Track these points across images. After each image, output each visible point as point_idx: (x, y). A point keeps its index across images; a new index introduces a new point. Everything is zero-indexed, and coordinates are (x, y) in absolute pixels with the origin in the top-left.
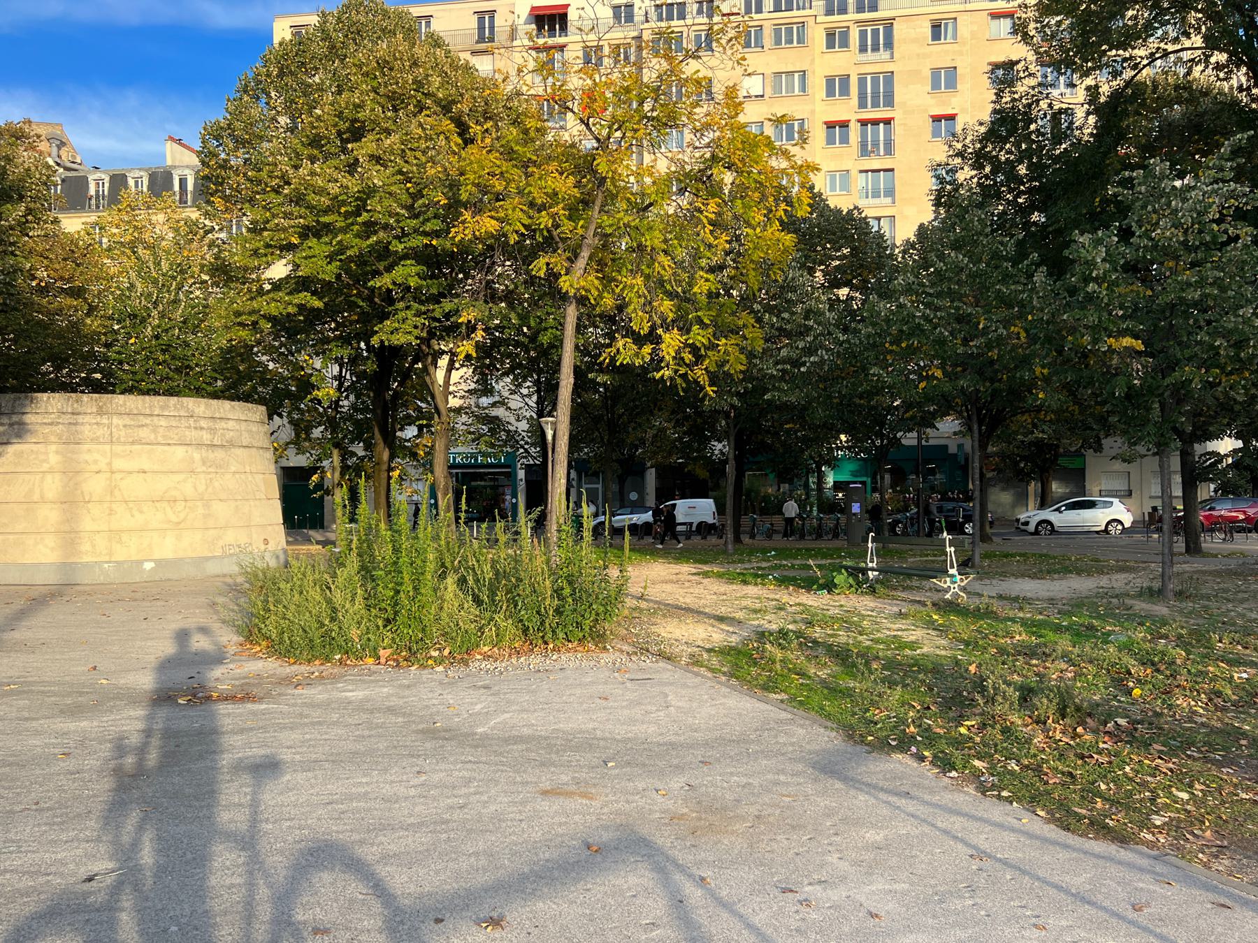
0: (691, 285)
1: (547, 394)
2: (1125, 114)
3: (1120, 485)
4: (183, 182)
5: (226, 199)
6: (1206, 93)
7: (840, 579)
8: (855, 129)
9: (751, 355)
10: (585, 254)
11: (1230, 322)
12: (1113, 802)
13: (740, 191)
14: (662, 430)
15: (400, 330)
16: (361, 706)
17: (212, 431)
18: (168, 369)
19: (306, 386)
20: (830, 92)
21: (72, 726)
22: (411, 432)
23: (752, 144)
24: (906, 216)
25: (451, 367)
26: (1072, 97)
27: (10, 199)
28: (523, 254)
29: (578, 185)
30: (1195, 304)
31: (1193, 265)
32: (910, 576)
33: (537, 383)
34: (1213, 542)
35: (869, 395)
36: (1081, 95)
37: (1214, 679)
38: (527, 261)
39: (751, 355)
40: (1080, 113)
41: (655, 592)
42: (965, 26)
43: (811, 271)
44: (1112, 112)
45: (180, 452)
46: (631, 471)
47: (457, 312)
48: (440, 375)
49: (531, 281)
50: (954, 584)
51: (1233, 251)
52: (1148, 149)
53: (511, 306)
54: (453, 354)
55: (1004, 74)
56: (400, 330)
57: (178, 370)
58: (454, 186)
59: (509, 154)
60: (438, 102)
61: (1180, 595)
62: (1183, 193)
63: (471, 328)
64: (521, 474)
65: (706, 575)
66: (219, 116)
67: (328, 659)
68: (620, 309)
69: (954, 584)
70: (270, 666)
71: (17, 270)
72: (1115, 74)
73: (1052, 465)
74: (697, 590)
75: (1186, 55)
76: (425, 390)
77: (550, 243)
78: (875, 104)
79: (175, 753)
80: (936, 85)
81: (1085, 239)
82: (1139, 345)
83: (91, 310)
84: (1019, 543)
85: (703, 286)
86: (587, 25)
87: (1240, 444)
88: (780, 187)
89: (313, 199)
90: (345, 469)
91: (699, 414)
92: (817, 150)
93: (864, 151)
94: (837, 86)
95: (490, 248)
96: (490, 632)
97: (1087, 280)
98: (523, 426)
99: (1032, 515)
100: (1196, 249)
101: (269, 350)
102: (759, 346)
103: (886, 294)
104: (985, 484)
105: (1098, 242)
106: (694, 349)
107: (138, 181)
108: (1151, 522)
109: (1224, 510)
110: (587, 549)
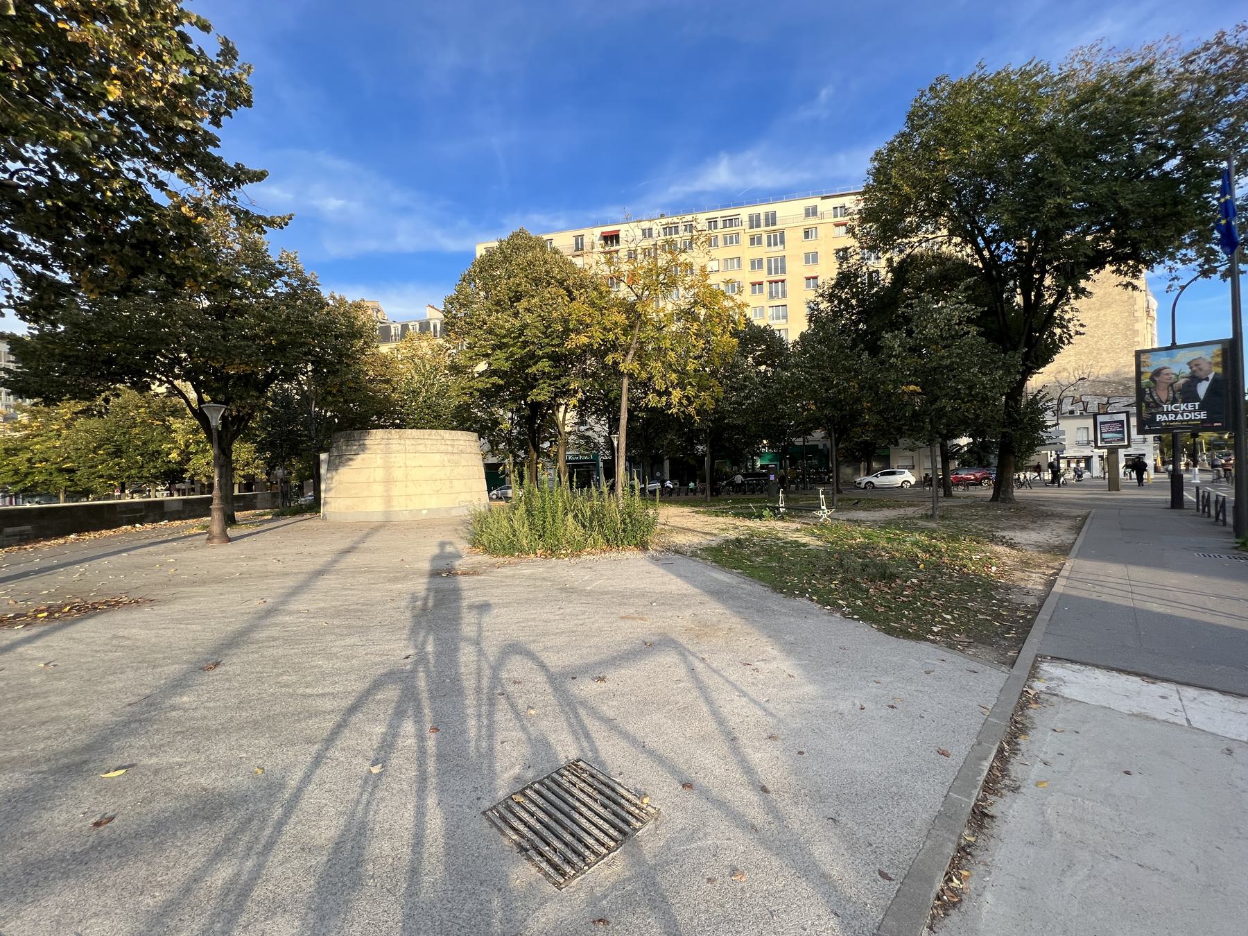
0: (685, 366)
1: (614, 425)
2: (907, 271)
3: (908, 463)
4: (435, 326)
5: (456, 333)
6: (949, 259)
7: (765, 513)
8: (766, 285)
9: (717, 400)
10: (632, 352)
11: (966, 375)
12: (913, 620)
13: (709, 318)
14: (672, 440)
15: (541, 394)
16: (529, 577)
17: (453, 446)
18: (431, 417)
19: (496, 423)
20: (753, 267)
21: (393, 587)
22: (546, 445)
23: (715, 295)
24: (793, 327)
25: (566, 411)
26: (880, 266)
27: (356, 337)
28: (600, 354)
29: (627, 318)
30: (947, 367)
31: (944, 347)
32: (801, 510)
33: (608, 418)
34: (958, 491)
35: (777, 419)
36: (883, 262)
37: (962, 558)
38: (603, 357)
39: (717, 400)
40: (883, 272)
41: (672, 521)
42: (821, 230)
43: (746, 357)
44: (900, 272)
45: (438, 456)
46: (657, 462)
47: (569, 383)
48: (560, 415)
49: (605, 367)
50: (824, 513)
51: (967, 339)
52: (920, 289)
53: (595, 380)
54: (567, 405)
55: (843, 255)
56: (541, 394)
57: (435, 417)
58: (566, 321)
59: (593, 304)
60: (557, 281)
61: (942, 517)
62: (939, 310)
63: (576, 392)
64: (601, 464)
65: (697, 512)
66: (452, 293)
67: (512, 555)
68: (650, 379)
69: (824, 513)
70: (486, 558)
71: (361, 371)
72: (901, 251)
73: (874, 454)
74: (694, 520)
75: (940, 239)
76: (553, 423)
77: (614, 347)
78: (776, 273)
79: (441, 601)
80: (807, 261)
81: (888, 336)
82: (918, 389)
83: (394, 389)
84: (856, 494)
85: (691, 367)
86: (630, 239)
87: (971, 440)
88: (729, 316)
89: (498, 331)
90: (515, 464)
91: (691, 431)
92: (747, 296)
93: (771, 296)
94: (756, 264)
95: (585, 351)
96: (590, 541)
97: (890, 356)
98: (602, 440)
99: (863, 479)
100: (947, 339)
101: (478, 406)
102: (721, 395)
103: (785, 368)
104: (838, 464)
105: (895, 337)
106: (688, 398)
107: (414, 327)
108: (925, 481)
109: (963, 474)
110: (638, 501)
